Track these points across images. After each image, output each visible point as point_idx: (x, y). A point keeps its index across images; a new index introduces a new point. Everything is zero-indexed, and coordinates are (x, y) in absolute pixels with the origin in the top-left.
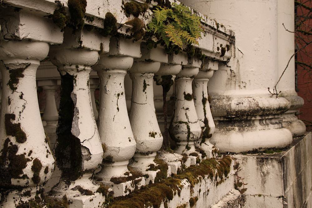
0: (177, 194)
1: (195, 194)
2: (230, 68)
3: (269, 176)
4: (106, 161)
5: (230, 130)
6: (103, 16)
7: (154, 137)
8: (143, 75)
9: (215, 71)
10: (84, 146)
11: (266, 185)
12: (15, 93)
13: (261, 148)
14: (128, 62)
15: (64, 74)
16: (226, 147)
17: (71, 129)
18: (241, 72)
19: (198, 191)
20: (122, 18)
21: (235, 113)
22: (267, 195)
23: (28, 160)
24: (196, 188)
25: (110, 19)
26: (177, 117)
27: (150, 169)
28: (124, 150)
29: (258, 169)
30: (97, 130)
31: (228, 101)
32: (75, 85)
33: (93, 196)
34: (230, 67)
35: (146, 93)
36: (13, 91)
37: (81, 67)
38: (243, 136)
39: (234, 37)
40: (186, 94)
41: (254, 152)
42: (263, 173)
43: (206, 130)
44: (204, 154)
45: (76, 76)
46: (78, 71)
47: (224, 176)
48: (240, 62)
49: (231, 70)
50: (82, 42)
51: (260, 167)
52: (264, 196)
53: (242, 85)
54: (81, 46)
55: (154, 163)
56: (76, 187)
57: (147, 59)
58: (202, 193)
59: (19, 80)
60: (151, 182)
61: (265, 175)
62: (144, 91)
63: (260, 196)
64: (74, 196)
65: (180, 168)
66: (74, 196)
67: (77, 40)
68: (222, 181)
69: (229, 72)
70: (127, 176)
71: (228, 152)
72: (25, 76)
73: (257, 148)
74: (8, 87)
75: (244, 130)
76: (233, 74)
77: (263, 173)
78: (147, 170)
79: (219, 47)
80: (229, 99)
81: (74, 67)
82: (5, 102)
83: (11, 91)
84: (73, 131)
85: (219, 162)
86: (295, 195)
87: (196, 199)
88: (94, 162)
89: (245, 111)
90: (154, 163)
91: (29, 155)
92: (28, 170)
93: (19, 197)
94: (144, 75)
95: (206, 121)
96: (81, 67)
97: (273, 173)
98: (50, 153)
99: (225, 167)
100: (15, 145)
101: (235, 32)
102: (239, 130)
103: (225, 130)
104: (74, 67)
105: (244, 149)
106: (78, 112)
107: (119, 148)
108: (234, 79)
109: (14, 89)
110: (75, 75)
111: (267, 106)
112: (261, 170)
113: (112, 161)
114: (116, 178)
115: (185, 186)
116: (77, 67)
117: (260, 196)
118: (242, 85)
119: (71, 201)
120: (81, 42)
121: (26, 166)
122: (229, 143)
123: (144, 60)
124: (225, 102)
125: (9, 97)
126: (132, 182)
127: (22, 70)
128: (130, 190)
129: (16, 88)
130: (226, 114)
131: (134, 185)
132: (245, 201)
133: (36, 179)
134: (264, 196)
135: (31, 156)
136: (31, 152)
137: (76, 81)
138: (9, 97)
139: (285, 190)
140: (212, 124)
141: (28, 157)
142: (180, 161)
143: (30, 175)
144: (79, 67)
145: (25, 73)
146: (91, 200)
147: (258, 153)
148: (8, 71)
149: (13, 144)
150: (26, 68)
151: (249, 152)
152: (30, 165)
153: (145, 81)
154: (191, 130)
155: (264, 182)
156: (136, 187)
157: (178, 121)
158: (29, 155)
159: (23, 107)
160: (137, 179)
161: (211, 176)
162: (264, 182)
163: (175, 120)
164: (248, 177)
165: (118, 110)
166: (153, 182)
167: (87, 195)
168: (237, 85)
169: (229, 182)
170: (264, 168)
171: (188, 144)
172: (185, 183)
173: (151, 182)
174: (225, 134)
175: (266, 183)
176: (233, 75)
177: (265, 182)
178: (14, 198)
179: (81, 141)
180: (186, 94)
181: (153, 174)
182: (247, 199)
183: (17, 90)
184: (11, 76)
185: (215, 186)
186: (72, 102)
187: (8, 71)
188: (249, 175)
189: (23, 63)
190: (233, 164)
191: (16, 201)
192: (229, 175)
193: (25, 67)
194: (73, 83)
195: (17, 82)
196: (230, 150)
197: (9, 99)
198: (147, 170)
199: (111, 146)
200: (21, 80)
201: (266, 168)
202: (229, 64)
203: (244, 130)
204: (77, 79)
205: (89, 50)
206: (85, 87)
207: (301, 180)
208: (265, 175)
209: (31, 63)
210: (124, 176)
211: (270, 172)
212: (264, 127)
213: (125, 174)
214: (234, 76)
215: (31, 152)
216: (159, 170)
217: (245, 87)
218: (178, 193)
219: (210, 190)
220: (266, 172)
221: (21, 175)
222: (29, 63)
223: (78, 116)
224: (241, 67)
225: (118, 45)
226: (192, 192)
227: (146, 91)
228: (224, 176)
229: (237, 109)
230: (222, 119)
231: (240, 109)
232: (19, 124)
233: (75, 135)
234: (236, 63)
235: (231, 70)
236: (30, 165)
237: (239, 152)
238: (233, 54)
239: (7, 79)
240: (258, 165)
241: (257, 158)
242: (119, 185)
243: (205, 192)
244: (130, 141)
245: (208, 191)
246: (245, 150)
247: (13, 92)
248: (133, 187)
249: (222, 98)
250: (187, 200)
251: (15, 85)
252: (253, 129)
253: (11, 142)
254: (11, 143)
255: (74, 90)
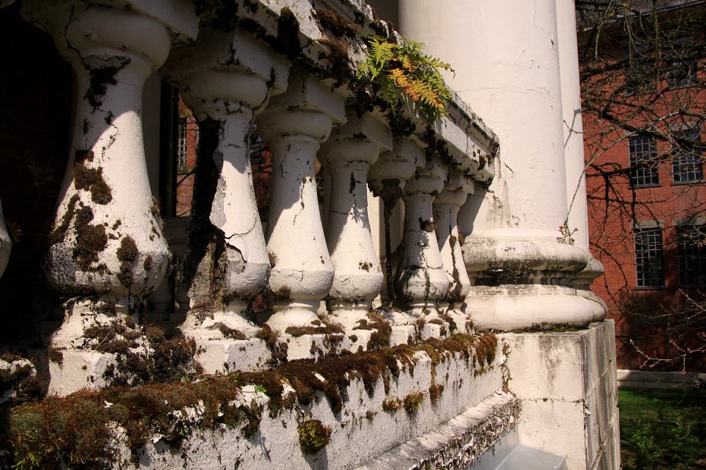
0: (407, 370)
1: (439, 380)
2: (492, 194)
3: (561, 366)
4: (280, 296)
5: (495, 294)
6: (277, 10)
7: (368, 271)
8: (350, 164)
9: (469, 195)
10: (231, 244)
11: (555, 382)
12: (97, 112)
13: (546, 323)
14: (322, 126)
15: (203, 117)
16: (488, 321)
17: (209, 215)
18: (511, 201)
19: (445, 375)
20: (311, 30)
21: (502, 265)
22: (558, 398)
23: (112, 237)
24: (441, 370)
25: (288, 21)
26: (408, 259)
27: (359, 328)
28: (311, 276)
29: (541, 355)
30: (259, 223)
31: (491, 245)
32: (221, 137)
33: (247, 341)
34: (493, 192)
35: (354, 195)
36: (95, 108)
37: (234, 107)
38: (516, 302)
39: (497, 145)
40: (424, 221)
41: (535, 329)
42: (551, 361)
43: (456, 287)
44: (453, 326)
45: (224, 122)
46: (228, 112)
47: (486, 364)
48: (509, 185)
49: (494, 197)
50: (235, 51)
51: (546, 351)
52: (552, 402)
53: (513, 221)
54: (232, 57)
55: (366, 318)
56: (216, 324)
57: (357, 133)
58: (451, 380)
59: (106, 88)
60: (361, 348)
61: (552, 365)
62: (351, 192)
63: (545, 400)
64: (210, 339)
65: (412, 335)
66: (210, 339)
67: (227, 47)
68: (482, 371)
69: (492, 200)
70: (316, 326)
71: (490, 330)
72: (119, 84)
73: (539, 322)
74: (87, 101)
75: (517, 294)
76: (498, 204)
77: (551, 361)
78: (354, 329)
79: (476, 152)
80: (492, 242)
81: (220, 104)
82: (78, 128)
83: (89, 108)
84: (214, 218)
85: (479, 338)
86: (598, 406)
87: (441, 388)
88: (250, 277)
89: (518, 262)
90: (366, 318)
91: (115, 227)
92: (109, 256)
93: (91, 313)
94: (352, 164)
95: (456, 274)
96: (234, 107)
97: (567, 361)
98: (159, 235)
99: (487, 347)
100: (88, 208)
101: (500, 139)
102: (510, 293)
103: (487, 293)
104: (220, 104)
105: (518, 324)
106: (224, 184)
107: (302, 271)
108: (499, 211)
109: (96, 105)
110: (222, 120)
111: (554, 254)
112: (548, 357)
113: (288, 297)
114: (295, 328)
115: (421, 360)
116: (227, 104)
117: (545, 400)
118: (513, 222)
119: (203, 347)
120: (233, 52)
121: (107, 247)
122: (494, 314)
123: (352, 136)
124: (485, 247)
125: (85, 120)
126: (326, 337)
127: (113, 71)
128: (320, 352)
129: (100, 104)
130: (486, 267)
131: (328, 344)
132: (521, 410)
133: (125, 275)
134: (552, 402)
135: (117, 230)
136: (119, 223)
137: (223, 130)
138: (85, 120)
139: (586, 392)
140: (465, 279)
141: (112, 232)
142: (414, 325)
143: (114, 265)
144: (229, 105)
145: (119, 76)
146: (243, 349)
147: (540, 331)
148: (88, 72)
149: (86, 204)
150: (121, 67)
151: (526, 330)
152: (113, 246)
153: (352, 175)
154: (431, 280)
155: (552, 377)
156: (333, 350)
157: (410, 265)
158: (115, 227)
159: (111, 140)
160: (334, 334)
161: (466, 355)
162: (552, 377)
163: (405, 261)
164: (526, 370)
165: (303, 207)
166: (365, 349)
167: (235, 338)
168: (505, 221)
169: (494, 375)
170: (553, 354)
171: (426, 299)
172: (422, 356)
173: (361, 348)
174: (487, 300)
175: (555, 379)
176: (499, 206)
177: (553, 377)
178: (82, 315)
179: (227, 235)
180: (424, 221)
181: (364, 336)
182: (524, 406)
183: (101, 108)
184: (92, 81)
185: (473, 375)
186: (215, 167)
187: (88, 72)
188: (528, 365)
189: (116, 57)
190: (500, 348)
191: (86, 321)
192: (493, 364)
193: (120, 65)
194: (219, 134)
195: (102, 91)
196: (495, 325)
197: (86, 124)
198: (354, 329)
199: (287, 268)
200: (111, 89)
201: (554, 354)
202: (491, 188)
203: (517, 294)
204: (225, 127)
205: (250, 73)
206: (241, 142)
207: (604, 386)
208: (553, 366)
209: (132, 58)
210: (311, 325)
211: (561, 359)
212: (549, 289)
213: (312, 323)
214: (500, 207)
215: (119, 223)
216: (375, 330)
217: (517, 224)
218: (410, 370)
219: (464, 380)
220: (554, 360)
221: (95, 265)
222: (128, 58)
223: (223, 192)
224: (510, 192)
225: (304, 87)
226: (433, 373)
227: (354, 192)
228: (486, 364)
229: (505, 258)
230: (481, 276)
231: (511, 257)
232: (100, 169)
233: (216, 225)
234: (502, 187)
235: (494, 197)
236: (113, 246)
237: (510, 329)
238: (497, 173)
239: (85, 82)
240: (541, 348)
241: (540, 337)
242: (299, 339)
243: (455, 380)
244: (323, 262)
245: (461, 381)
246: (521, 326)
247: (94, 111)
248: (327, 347)
249: (480, 241)
250: (425, 387)
251: (98, 98)
252: (532, 292)
253: (81, 200)
254: (81, 204)
255: (220, 145)
